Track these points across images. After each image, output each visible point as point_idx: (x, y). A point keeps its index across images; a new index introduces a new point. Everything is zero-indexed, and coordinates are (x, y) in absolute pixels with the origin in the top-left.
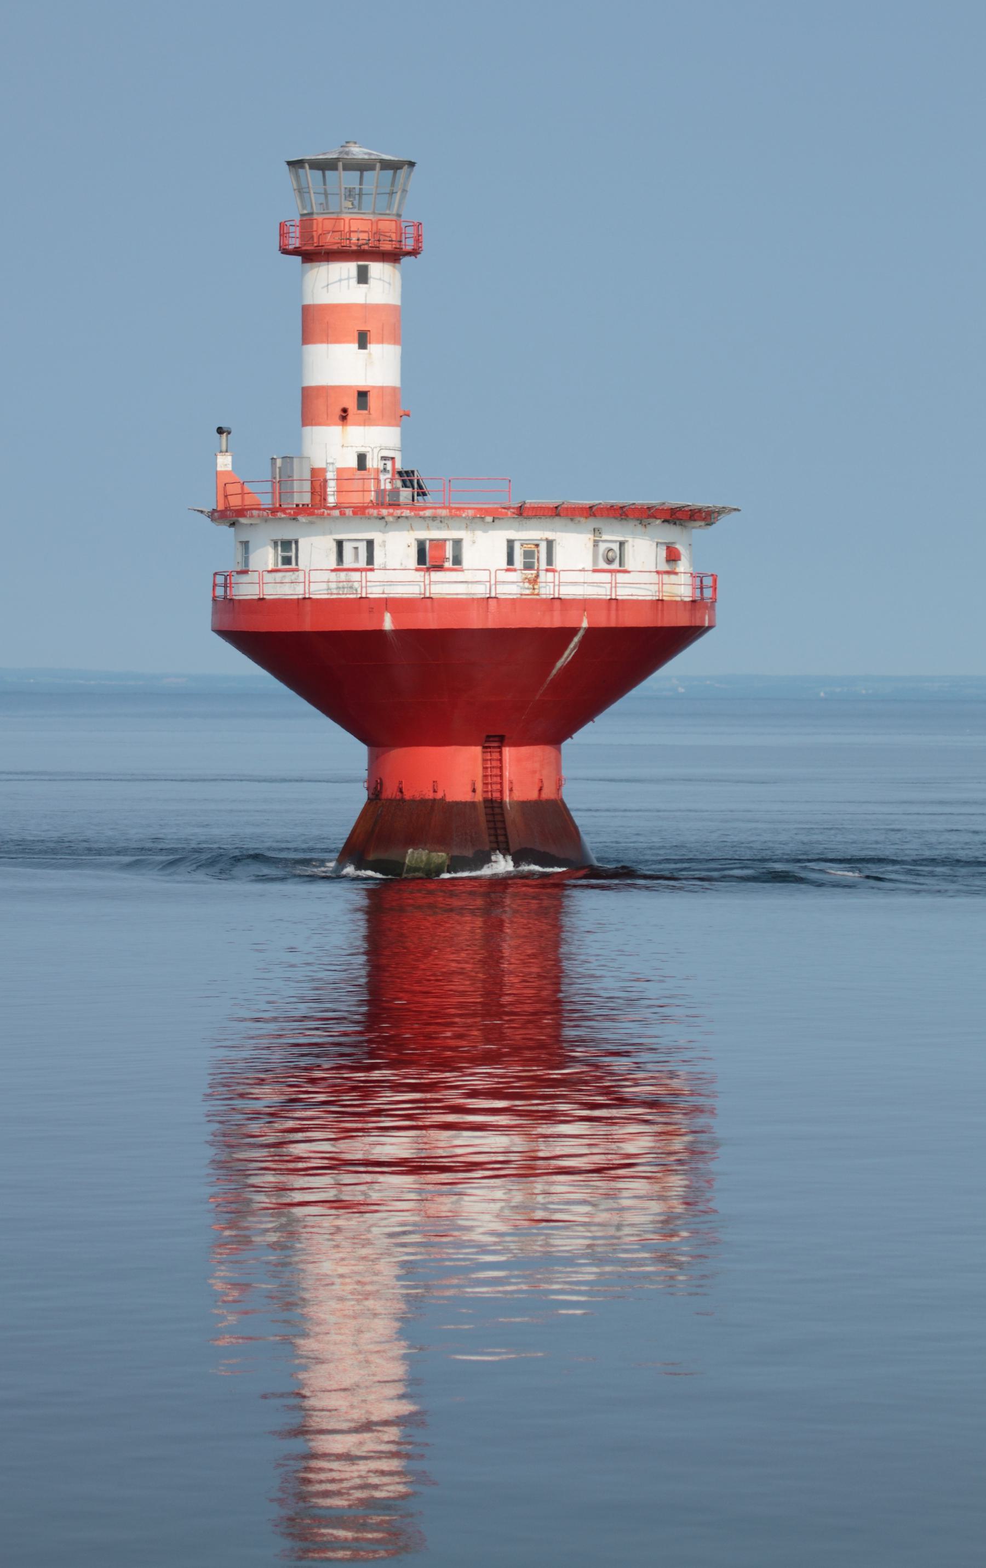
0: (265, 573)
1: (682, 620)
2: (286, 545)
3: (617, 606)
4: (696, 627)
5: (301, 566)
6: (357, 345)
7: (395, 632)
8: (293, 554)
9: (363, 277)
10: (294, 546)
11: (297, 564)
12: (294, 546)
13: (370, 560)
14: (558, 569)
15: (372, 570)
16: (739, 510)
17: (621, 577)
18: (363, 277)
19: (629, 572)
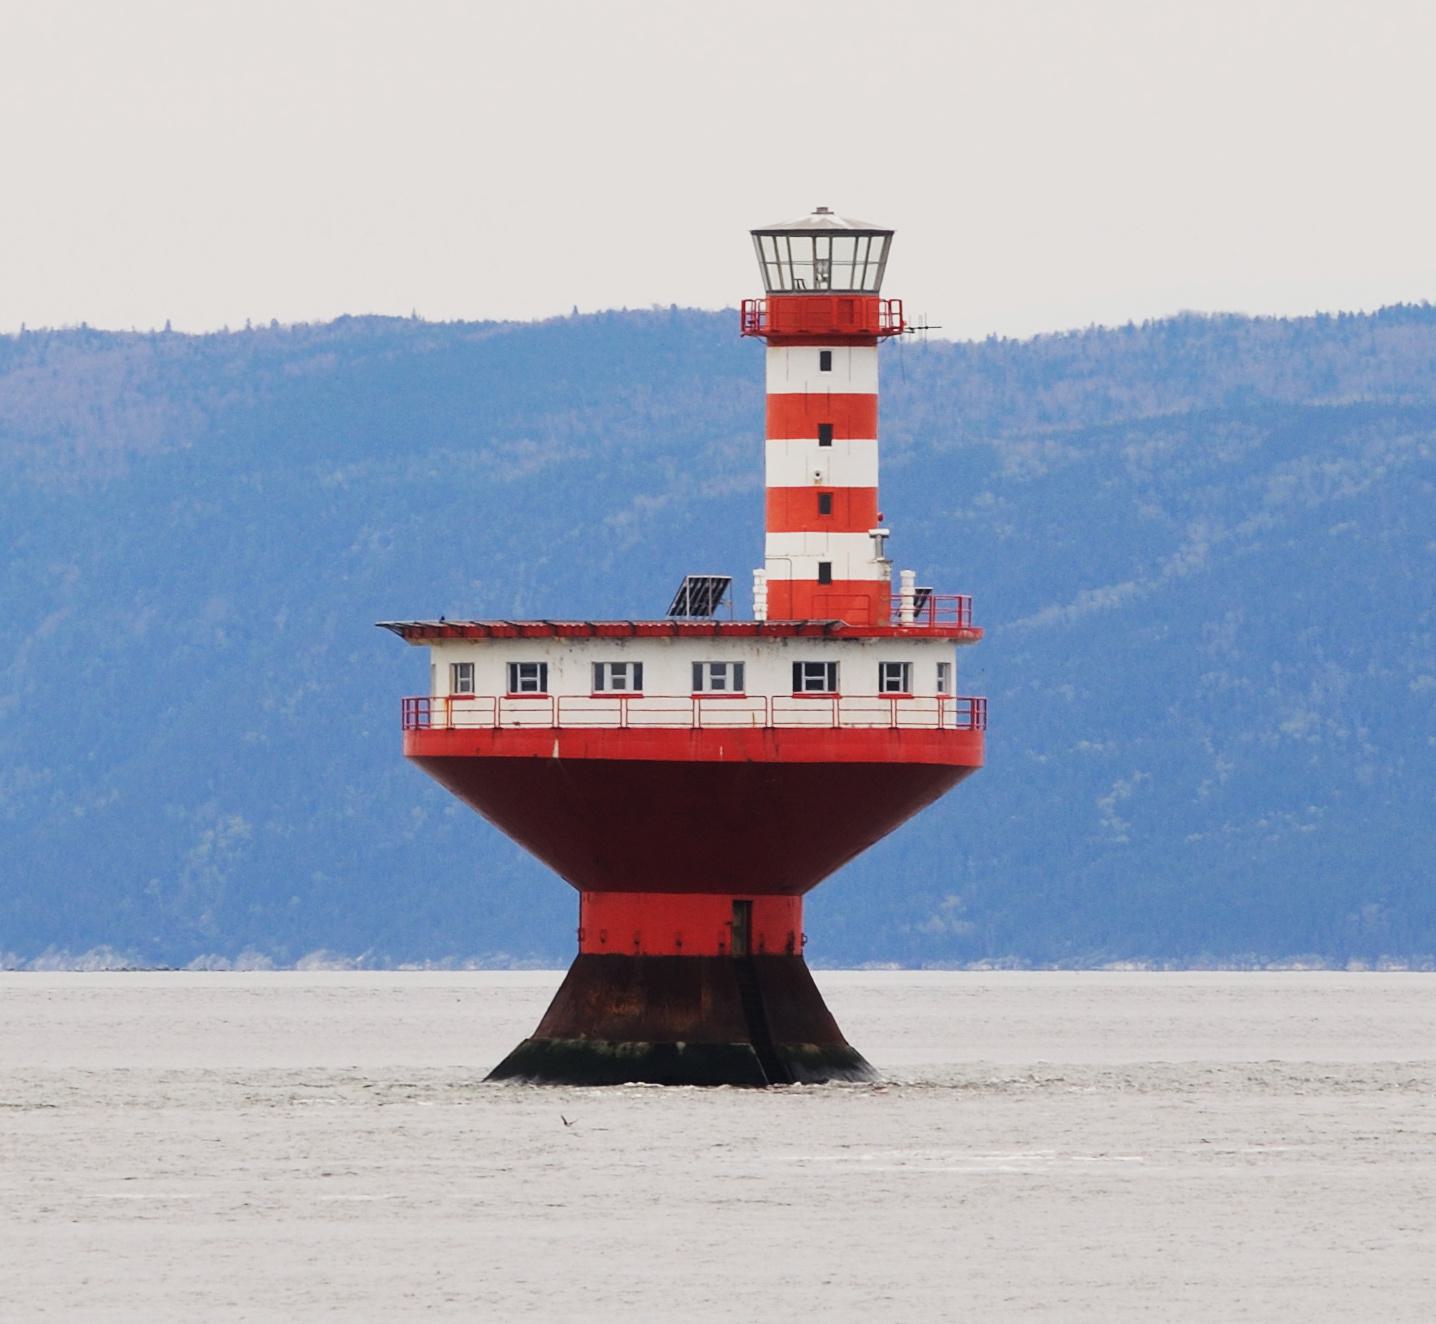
0: (502, 699)
1: (931, 755)
2: (894, 669)
3: (899, 736)
4: (957, 767)
5: (549, 692)
6: (817, 441)
7: (559, 759)
8: (901, 679)
9: (826, 363)
10: (471, 667)
11: (473, 691)
12: (471, 667)
13: (638, 684)
14: (842, 694)
15: (640, 696)
16: (408, 632)
17: (901, 703)
18: (826, 363)
19: (912, 698)
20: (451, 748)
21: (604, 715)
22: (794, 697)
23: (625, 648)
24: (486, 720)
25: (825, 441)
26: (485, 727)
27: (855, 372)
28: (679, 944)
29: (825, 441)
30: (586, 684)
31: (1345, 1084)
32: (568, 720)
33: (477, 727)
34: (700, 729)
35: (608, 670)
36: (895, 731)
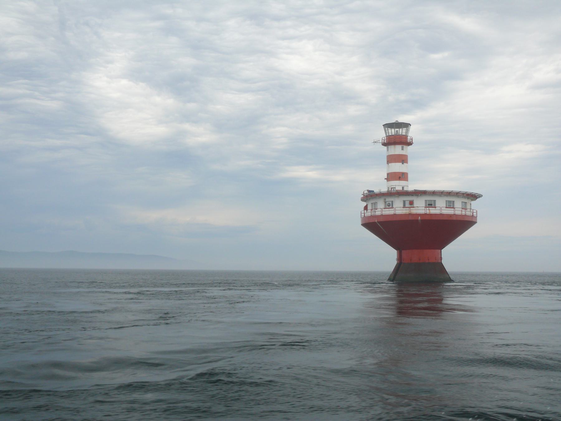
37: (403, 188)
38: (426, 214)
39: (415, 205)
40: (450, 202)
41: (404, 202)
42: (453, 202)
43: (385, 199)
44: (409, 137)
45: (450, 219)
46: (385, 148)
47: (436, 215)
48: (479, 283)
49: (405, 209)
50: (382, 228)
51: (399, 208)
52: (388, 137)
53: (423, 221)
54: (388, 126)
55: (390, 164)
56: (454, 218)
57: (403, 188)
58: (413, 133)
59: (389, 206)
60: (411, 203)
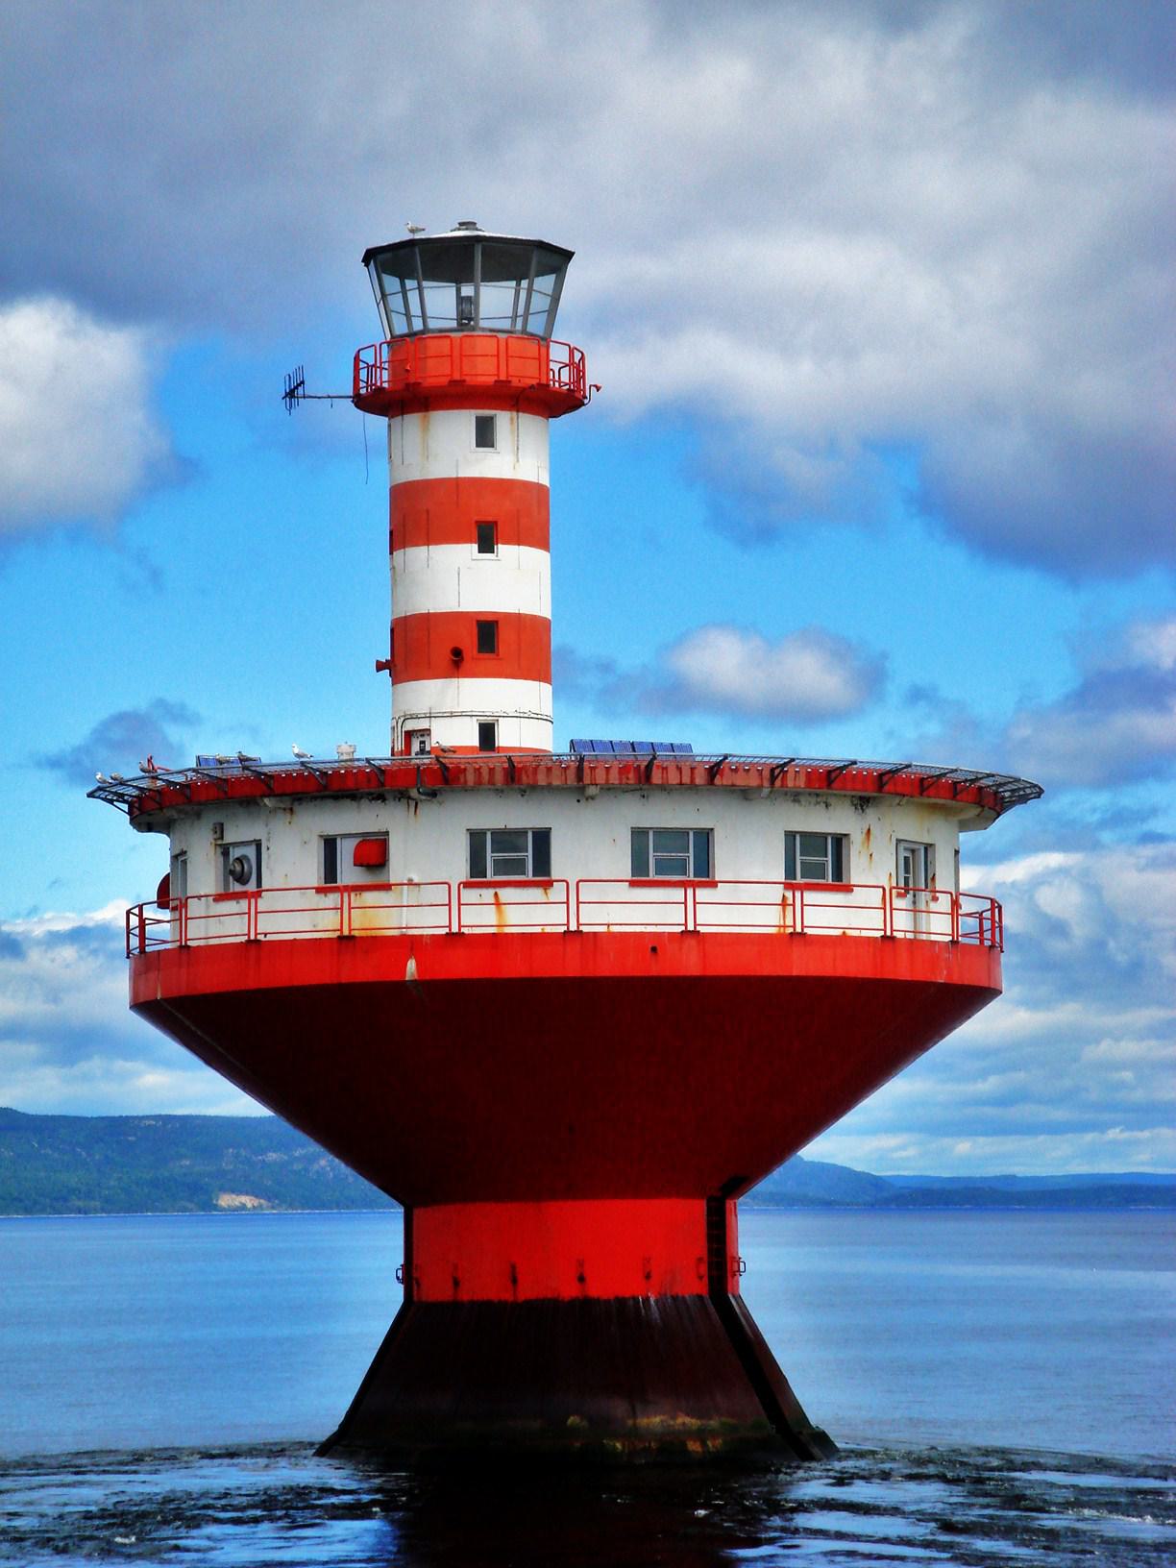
9: (485, 436)
17: (703, 894)
18: (485, 436)
20: (183, 983)
21: (656, 912)
22: (633, 884)
23: (295, 818)
24: (430, 922)
25: (486, 546)
26: (548, 930)
27: (521, 453)
28: (456, 1283)
29: (486, 546)
30: (312, 872)
31: (981, 1333)
32: (596, 918)
33: (538, 930)
34: (579, 932)
35: (346, 851)
36: (692, 942)
37: (487, 732)
38: (454, 939)
39: (396, 871)
40: (812, 842)
41: (330, 845)
42: (839, 841)
43: (219, 830)
44: (558, 354)
45: (656, 969)
46: (378, 423)
47: (843, 942)
48: (1090, 1466)
49: (333, 899)
50: (337, 1051)
51: (430, 892)
52: (405, 345)
53: (427, 988)
54: (400, 261)
55: (417, 554)
56: (691, 964)
57: (487, 732)
58: (584, 323)
59: (242, 879)
60: (374, 854)
